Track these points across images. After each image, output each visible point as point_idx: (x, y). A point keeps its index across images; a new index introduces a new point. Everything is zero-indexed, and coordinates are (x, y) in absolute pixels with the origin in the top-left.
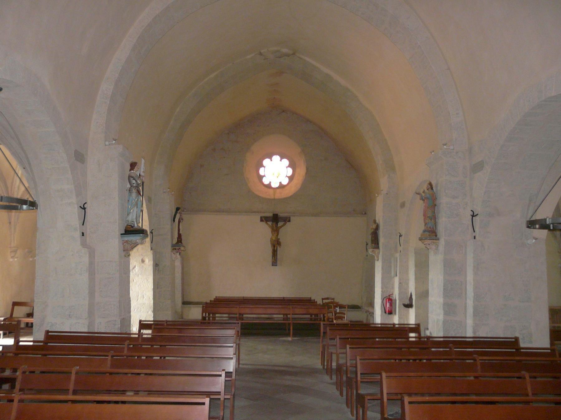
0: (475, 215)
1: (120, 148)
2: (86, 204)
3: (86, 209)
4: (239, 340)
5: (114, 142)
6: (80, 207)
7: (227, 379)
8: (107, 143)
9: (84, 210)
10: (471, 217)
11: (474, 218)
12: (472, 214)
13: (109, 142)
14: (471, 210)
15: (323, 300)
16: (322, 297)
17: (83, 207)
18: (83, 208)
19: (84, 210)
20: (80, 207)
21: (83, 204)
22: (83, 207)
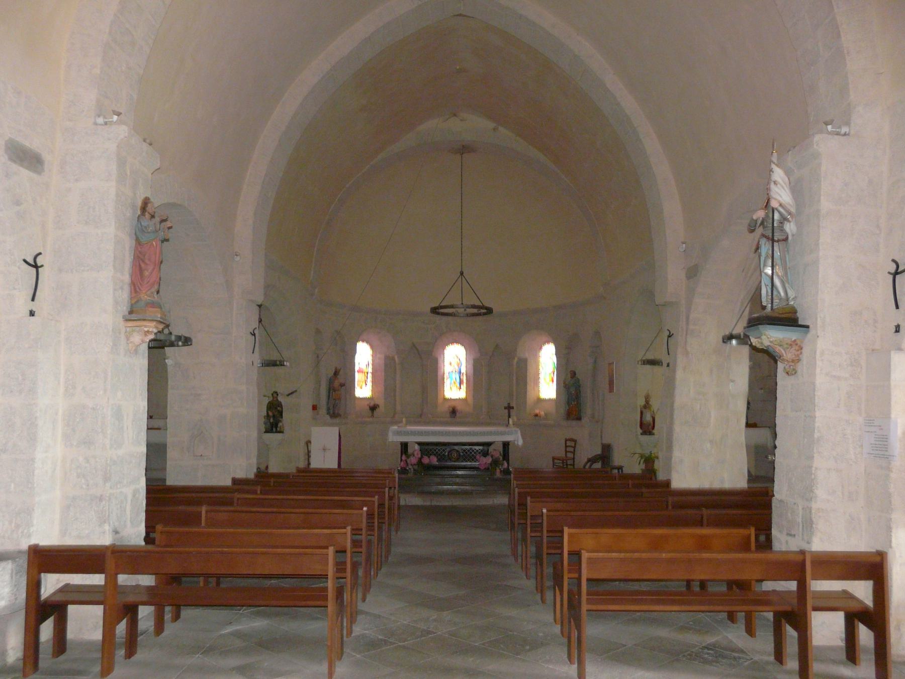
0: (899, 270)
1: (641, 472)
2: (40, 256)
3: (40, 269)
4: (571, 444)
5: (115, 118)
6: (25, 261)
7: (369, 521)
8: (100, 120)
9: (34, 270)
10: (891, 277)
11: (898, 277)
12: (893, 271)
13: (105, 117)
14: (894, 261)
15: (567, 442)
16: (233, 475)
17: (252, 332)
18: (34, 264)
19: (254, 337)
20: (25, 261)
21: (253, 329)
22: (252, 332)
